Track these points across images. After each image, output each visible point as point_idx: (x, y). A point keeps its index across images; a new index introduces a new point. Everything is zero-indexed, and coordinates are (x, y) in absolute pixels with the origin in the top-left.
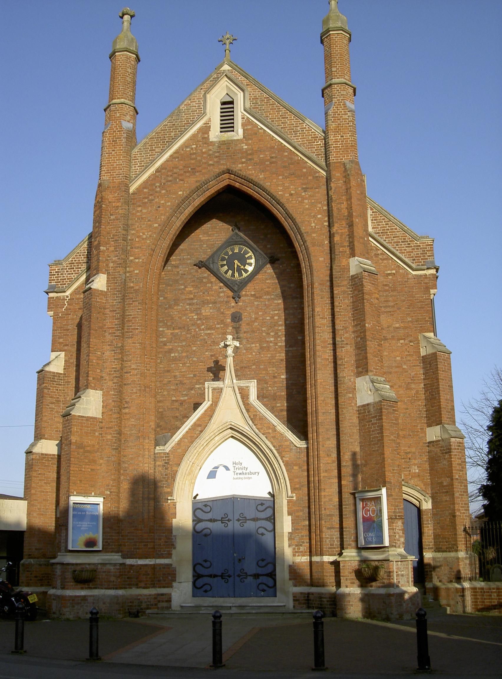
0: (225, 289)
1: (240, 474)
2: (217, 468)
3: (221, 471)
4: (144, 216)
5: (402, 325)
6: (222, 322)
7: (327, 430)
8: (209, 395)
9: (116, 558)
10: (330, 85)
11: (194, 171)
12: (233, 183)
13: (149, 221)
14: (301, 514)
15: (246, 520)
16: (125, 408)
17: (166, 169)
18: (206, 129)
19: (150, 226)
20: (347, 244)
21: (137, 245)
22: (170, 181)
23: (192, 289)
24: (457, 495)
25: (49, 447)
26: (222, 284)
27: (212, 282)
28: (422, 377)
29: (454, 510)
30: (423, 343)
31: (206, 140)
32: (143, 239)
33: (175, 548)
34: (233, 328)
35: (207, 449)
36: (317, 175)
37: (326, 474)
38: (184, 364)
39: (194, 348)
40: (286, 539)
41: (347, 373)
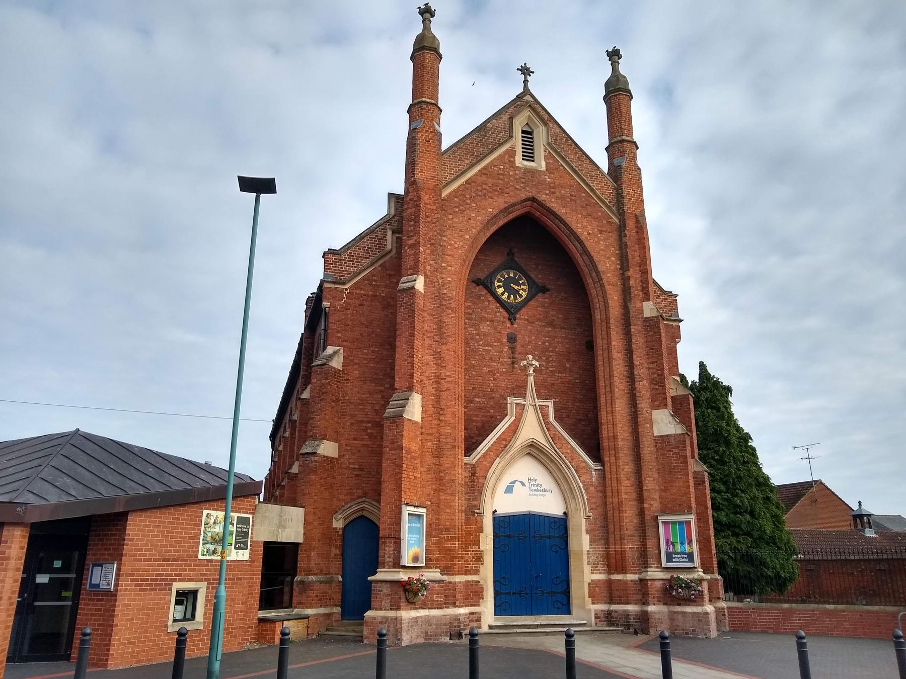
0: (501, 310)
2: (514, 483)
6: (499, 341)
8: (512, 410)
9: (433, 574)
11: (502, 192)
18: (512, 153)
19: (462, 236)
21: (449, 253)
32: (455, 248)
33: (482, 564)
41: (644, 404)
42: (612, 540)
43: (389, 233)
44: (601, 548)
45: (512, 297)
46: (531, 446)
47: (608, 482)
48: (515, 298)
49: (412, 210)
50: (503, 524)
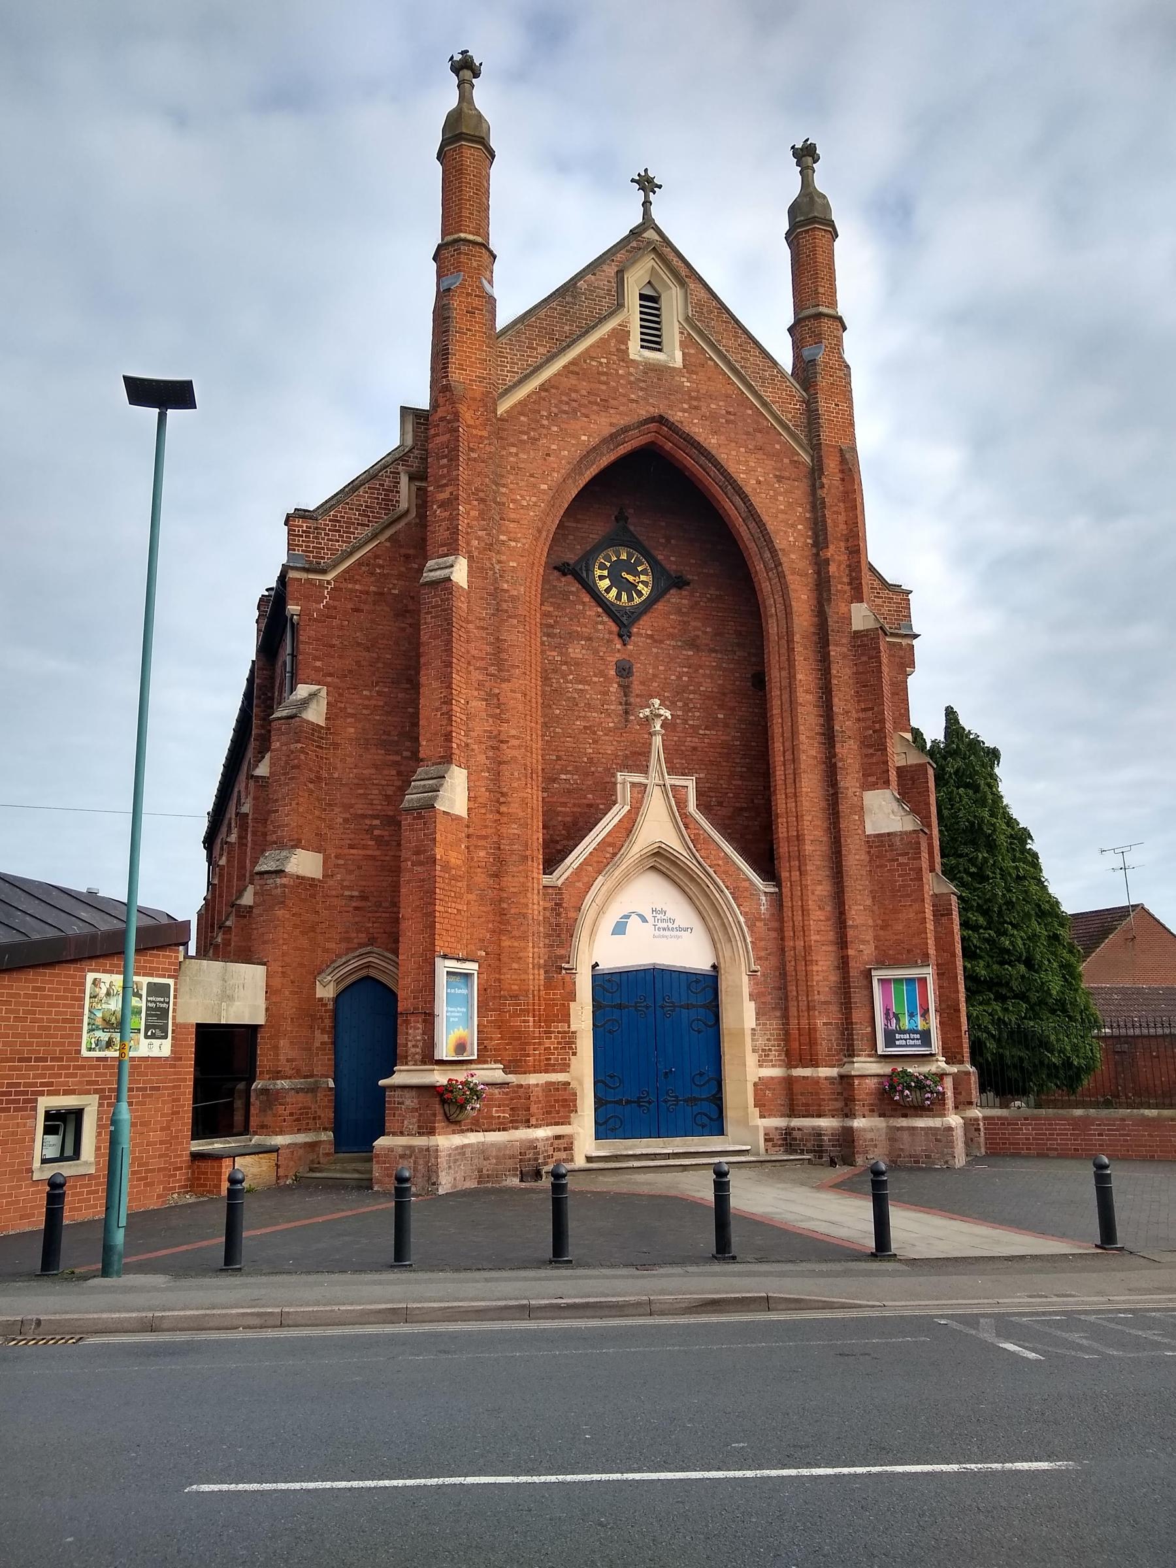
0: (606, 619)
1: (664, 929)
2: (628, 917)
3: (634, 921)
4: (522, 466)
6: (602, 674)
9: (493, 1073)
11: (605, 405)
12: (661, 441)
13: (532, 476)
15: (674, 1006)
17: (557, 388)
18: (622, 335)
19: (534, 486)
21: (513, 516)
22: (565, 412)
23: (551, 609)
26: (600, 610)
27: (584, 603)
33: (574, 1054)
34: (620, 686)
36: (796, 458)
37: (818, 937)
39: (558, 712)
41: (849, 782)
42: (793, 1011)
43: (404, 480)
44: (774, 1024)
45: (624, 596)
47: (787, 913)
48: (630, 598)
49: (444, 438)
50: (608, 985)
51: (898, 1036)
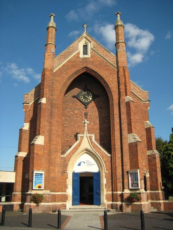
0: (82, 105)
2: (81, 162)
3: (82, 163)
5: (139, 118)
6: (81, 115)
7: (118, 151)
9: (48, 192)
10: (118, 42)
11: (75, 67)
14: (109, 178)
16: (51, 142)
18: (79, 53)
20: (124, 92)
22: (67, 69)
24: (158, 172)
25: (23, 154)
26: (81, 103)
28: (146, 135)
29: (157, 177)
30: (146, 124)
31: (78, 57)
33: (67, 189)
35: (78, 156)
37: (118, 165)
38: (69, 128)
40: (104, 186)
45: (86, 100)
46: (86, 150)
48: (87, 100)
51: (133, 185)
